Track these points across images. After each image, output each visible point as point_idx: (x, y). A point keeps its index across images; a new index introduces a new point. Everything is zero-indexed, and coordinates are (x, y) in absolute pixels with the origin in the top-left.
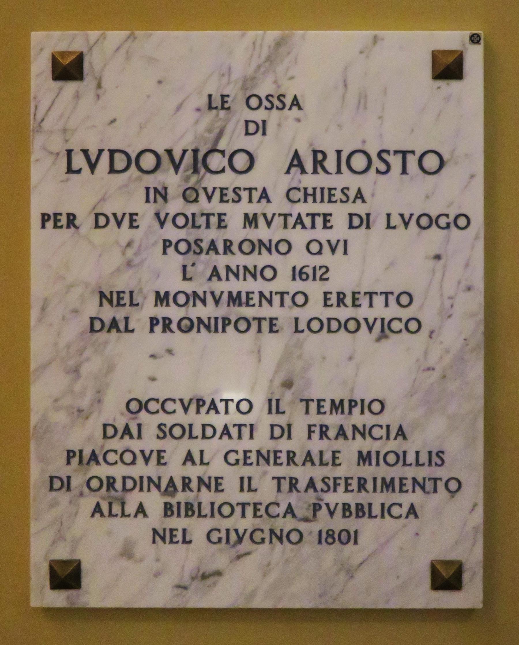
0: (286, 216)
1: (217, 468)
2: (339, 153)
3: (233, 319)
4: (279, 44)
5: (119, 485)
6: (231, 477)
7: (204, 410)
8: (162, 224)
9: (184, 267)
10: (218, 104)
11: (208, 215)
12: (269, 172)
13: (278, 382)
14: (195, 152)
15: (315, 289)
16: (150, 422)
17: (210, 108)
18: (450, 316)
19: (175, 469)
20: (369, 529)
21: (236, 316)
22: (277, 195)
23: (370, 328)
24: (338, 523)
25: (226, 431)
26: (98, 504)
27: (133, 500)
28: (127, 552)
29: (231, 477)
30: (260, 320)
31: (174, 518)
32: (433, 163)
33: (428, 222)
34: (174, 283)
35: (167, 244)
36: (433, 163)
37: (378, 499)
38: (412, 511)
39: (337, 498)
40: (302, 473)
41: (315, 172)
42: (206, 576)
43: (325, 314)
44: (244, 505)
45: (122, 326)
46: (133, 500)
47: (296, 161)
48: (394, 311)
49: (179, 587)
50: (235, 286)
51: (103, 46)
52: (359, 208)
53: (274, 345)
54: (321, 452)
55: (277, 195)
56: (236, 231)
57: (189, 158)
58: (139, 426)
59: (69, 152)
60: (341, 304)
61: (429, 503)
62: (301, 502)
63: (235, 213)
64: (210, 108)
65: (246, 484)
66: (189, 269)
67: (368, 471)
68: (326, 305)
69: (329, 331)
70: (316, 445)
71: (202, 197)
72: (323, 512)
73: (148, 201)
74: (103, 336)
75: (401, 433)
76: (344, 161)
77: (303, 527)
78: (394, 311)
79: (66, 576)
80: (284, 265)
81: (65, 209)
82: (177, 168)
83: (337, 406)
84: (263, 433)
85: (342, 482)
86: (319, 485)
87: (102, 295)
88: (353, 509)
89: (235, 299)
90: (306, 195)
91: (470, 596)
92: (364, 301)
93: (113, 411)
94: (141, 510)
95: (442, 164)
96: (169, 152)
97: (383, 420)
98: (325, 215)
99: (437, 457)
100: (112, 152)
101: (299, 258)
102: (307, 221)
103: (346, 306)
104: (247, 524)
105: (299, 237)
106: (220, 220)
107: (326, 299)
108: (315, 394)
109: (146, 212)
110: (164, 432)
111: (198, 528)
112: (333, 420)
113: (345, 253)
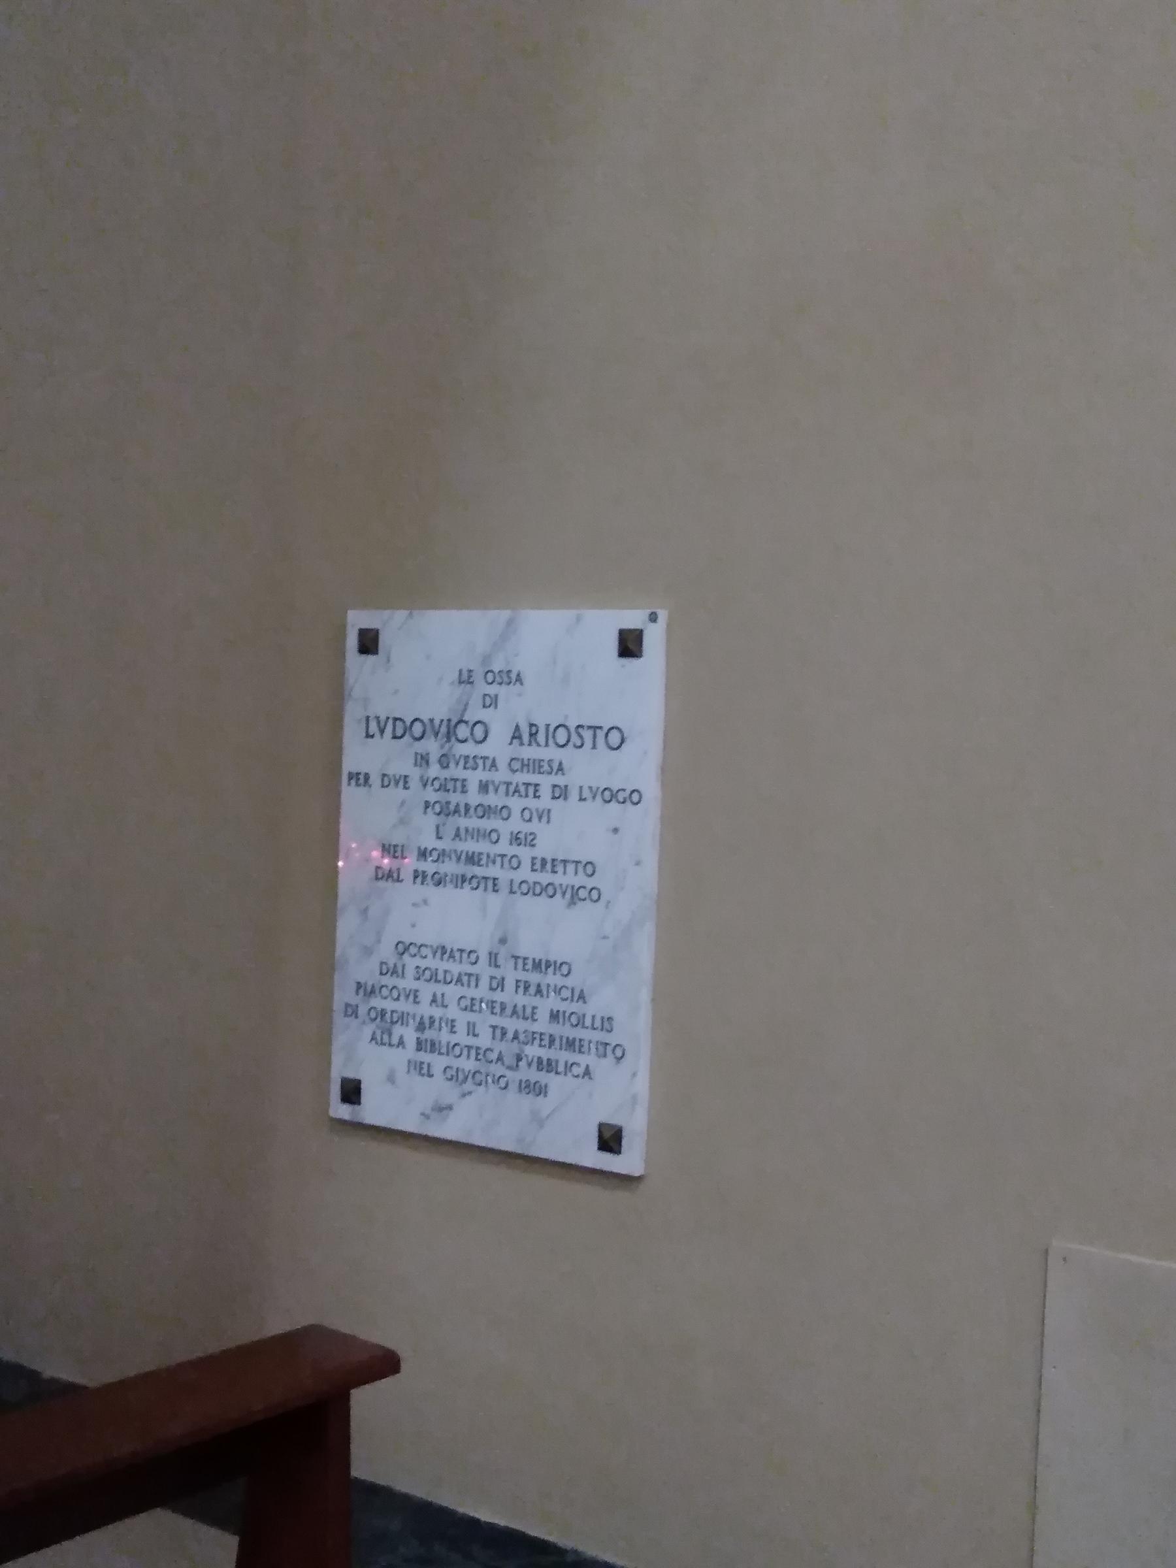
0: (508, 784)
1: (453, 1012)
2: (548, 726)
3: (469, 876)
4: (510, 622)
5: (388, 1015)
6: (462, 1019)
7: (446, 956)
8: (425, 785)
9: (438, 827)
10: (466, 679)
11: (456, 780)
12: (498, 747)
13: (496, 939)
14: (449, 720)
15: (525, 853)
16: (411, 963)
17: (460, 682)
18: (622, 888)
19: (425, 1009)
20: (554, 1082)
21: (471, 875)
22: (502, 764)
23: (564, 894)
24: (534, 1075)
25: (459, 980)
26: (374, 1033)
27: (398, 1031)
28: (391, 1079)
29: (462, 1019)
30: (486, 878)
31: (422, 1053)
32: (614, 738)
33: (610, 796)
34: (429, 842)
35: (427, 805)
36: (614, 738)
37: (564, 1056)
38: (587, 1073)
39: (533, 1051)
40: (512, 1025)
41: (530, 745)
42: (443, 1109)
43: (532, 877)
44: (469, 1048)
45: (395, 875)
46: (398, 1031)
47: (516, 736)
48: (580, 880)
49: (423, 1114)
50: (470, 846)
51: (391, 624)
52: (560, 780)
53: (495, 902)
54: (524, 1007)
55: (502, 764)
56: (474, 797)
57: (444, 729)
58: (404, 966)
59: (368, 718)
60: (533, 743)
61: (602, 1067)
62: (508, 1049)
63: (474, 778)
64: (460, 682)
65: (472, 1030)
66: (441, 828)
67: (556, 1029)
68: (533, 870)
69: (534, 894)
70: (521, 1000)
71: (452, 765)
72: (523, 1064)
73: (416, 764)
74: (382, 884)
75: (582, 997)
76: (551, 732)
77: (509, 1073)
78: (580, 880)
79: (352, 1092)
80: (506, 828)
81: (364, 770)
82: (436, 734)
83: (537, 965)
84: (484, 982)
85: (537, 1036)
86: (522, 1037)
87: (384, 846)
88: (545, 1063)
89: (472, 859)
90: (523, 765)
91: (628, 1162)
92: (560, 868)
93: (386, 952)
94: (401, 1043)
95: (623, 741)
96: (432, 720)
97: (569, 982)
98: (536, 785)
99: (607, 1024)
100: (396, 719)
101: (516, 824)
102: (522, 789)
103: (539, 745)
104: (469, 1065)
105: (516, 804)
106: (464, 786)
107: (533, 864)
108: (522, 953)
109: (415, 773)
110: (419, 974)
111: (438, 1062)
112: (534, 978)
113: (548, 822)
